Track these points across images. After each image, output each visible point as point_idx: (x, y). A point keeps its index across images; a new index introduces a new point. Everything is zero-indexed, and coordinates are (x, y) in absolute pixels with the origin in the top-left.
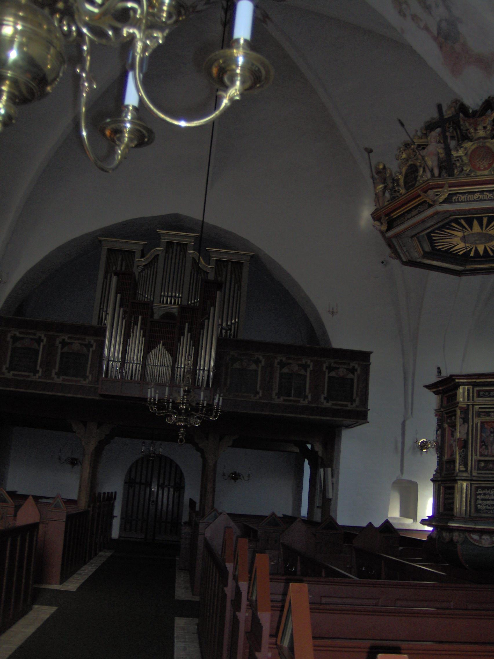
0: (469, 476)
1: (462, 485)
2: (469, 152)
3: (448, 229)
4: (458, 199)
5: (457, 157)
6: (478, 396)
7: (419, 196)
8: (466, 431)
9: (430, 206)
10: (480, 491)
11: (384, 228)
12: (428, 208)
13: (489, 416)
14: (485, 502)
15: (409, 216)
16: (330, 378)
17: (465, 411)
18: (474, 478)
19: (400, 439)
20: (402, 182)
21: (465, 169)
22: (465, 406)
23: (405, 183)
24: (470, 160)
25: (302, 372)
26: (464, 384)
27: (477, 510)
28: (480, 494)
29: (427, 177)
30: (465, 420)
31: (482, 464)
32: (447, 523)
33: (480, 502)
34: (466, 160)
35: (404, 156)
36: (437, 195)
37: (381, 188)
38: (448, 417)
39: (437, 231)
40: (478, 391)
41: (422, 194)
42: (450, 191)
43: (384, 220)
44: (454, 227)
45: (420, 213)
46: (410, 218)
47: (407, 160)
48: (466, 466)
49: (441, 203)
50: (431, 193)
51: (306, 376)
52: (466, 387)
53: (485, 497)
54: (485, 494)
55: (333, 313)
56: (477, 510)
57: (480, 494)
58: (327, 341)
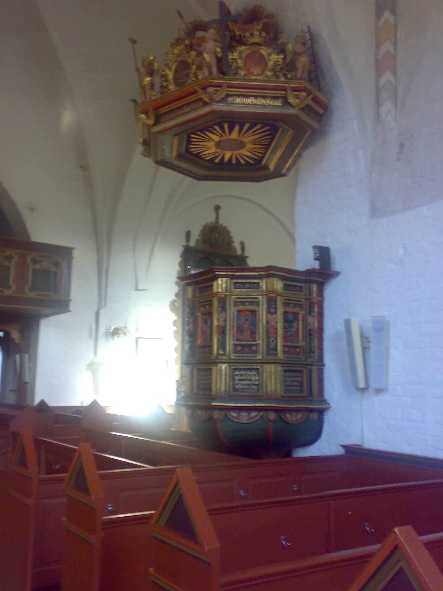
0: (227, 358)
1: (221, 367)
2: (244, 56)
3: (209, 131)
4: (233, 101)
5: (232, 59)
6: (235, 288)
7: (196, 92)
8: (224, 319)
9: (205, 104)
10: (237, 373)
11: (150, 122)
12: (202, 107)
13: (244, 305)
14: (241, 382)
15: (180, 112)
16: (34, 270)
17: (223, 301)
18: (232, 361)
19: (94, 327)
20: (171, 76)
21: (240, 72)
22: (223, 296)
23: (175, 78)
24: (245, 63)
25: (6, 263)
26: (222, 276)
27: (235, 390)
28: (237, 375)
29: (204, 74)
30: (224, 309)
31: (239, 348)
32: (210, 403)
33: (237, 382)
34: (240, 62)
35: (176, 51)
36: (216, 94)
37: (149, 81)
38: (201, 306)
39: (199, 133)
40: (235, 283)
41: (200, 91)
42: (227, 91)
43: (152, 114)
44: (216, 130)
45: (193, 110)
46: (181, 115)
47: (178, 56)
48: (224, 349)
49: (217, 102)
50: (210, 90)
51: (9, 268)
52: (224, 279)
53: (242, 378)
54: (241, 375)
55: (32, 210)
56: (235, 390)
57: (237, 375)
58: (28, 237)
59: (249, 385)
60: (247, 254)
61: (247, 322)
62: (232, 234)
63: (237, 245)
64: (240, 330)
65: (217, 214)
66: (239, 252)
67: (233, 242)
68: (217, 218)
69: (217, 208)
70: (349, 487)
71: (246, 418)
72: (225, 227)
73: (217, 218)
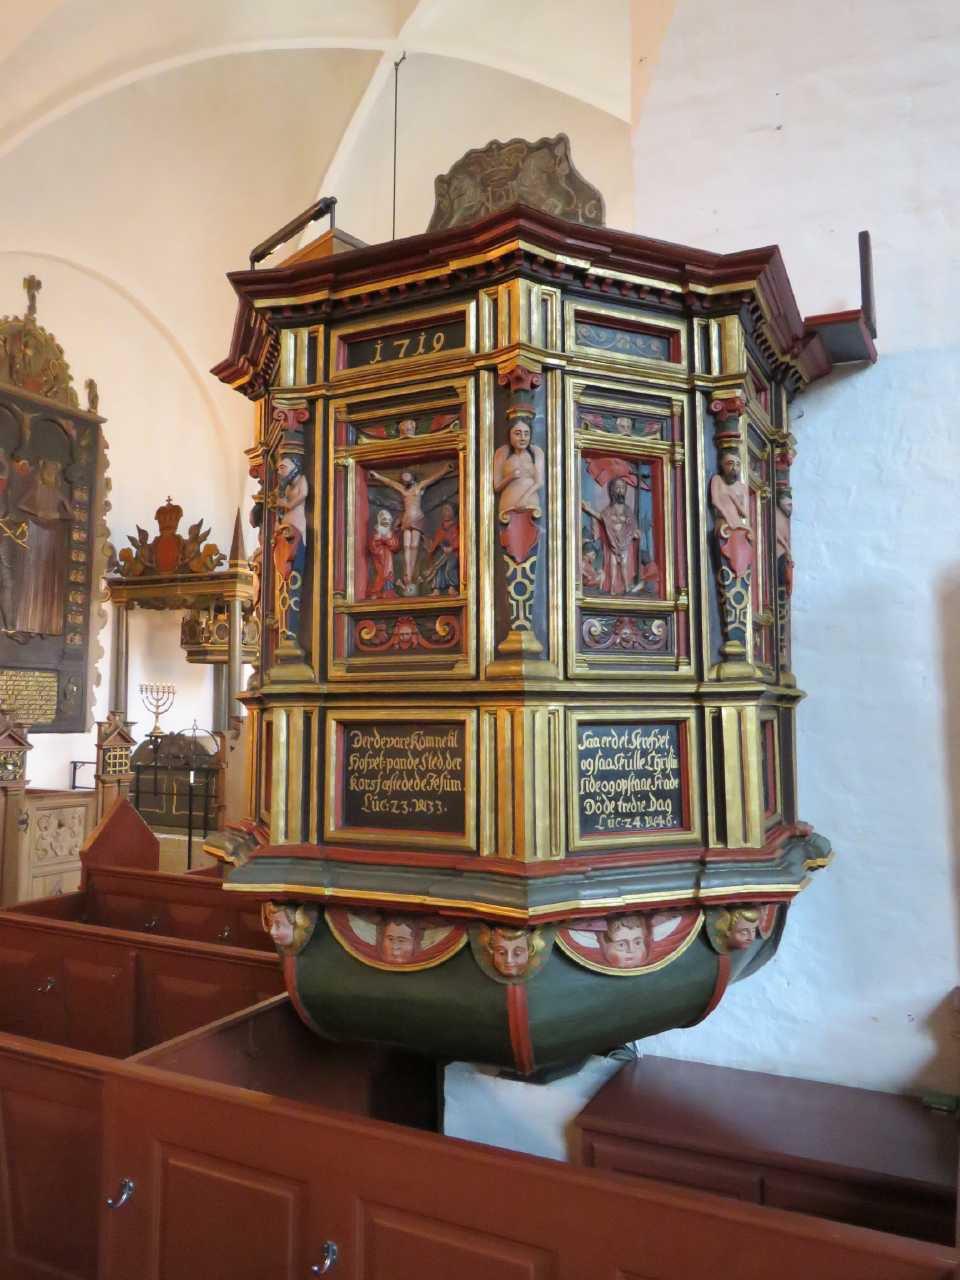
14: (611, 786)
59: (643, 796)
60: (101, 412)
61: (619, 508)
62: (67, 358)
63: (78, 387)
64: (597, 540)
65: (32, 298)
66: (83, 404)
67: (71, 378)
68: (32, 308)
69: (32, 285)
70: (122, 865)
71: (639, 951)
72: (52, 337)
73: (32, 308)
